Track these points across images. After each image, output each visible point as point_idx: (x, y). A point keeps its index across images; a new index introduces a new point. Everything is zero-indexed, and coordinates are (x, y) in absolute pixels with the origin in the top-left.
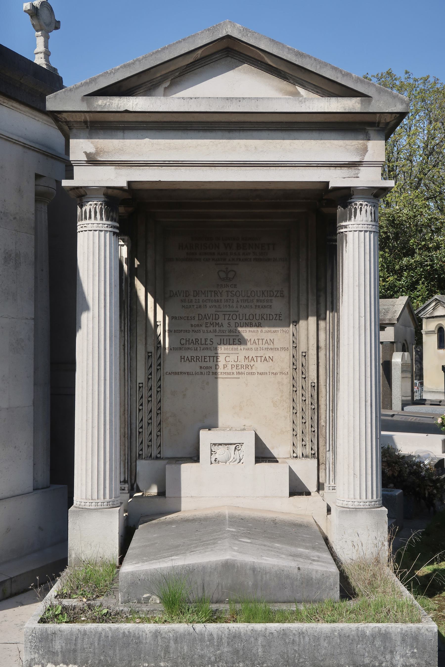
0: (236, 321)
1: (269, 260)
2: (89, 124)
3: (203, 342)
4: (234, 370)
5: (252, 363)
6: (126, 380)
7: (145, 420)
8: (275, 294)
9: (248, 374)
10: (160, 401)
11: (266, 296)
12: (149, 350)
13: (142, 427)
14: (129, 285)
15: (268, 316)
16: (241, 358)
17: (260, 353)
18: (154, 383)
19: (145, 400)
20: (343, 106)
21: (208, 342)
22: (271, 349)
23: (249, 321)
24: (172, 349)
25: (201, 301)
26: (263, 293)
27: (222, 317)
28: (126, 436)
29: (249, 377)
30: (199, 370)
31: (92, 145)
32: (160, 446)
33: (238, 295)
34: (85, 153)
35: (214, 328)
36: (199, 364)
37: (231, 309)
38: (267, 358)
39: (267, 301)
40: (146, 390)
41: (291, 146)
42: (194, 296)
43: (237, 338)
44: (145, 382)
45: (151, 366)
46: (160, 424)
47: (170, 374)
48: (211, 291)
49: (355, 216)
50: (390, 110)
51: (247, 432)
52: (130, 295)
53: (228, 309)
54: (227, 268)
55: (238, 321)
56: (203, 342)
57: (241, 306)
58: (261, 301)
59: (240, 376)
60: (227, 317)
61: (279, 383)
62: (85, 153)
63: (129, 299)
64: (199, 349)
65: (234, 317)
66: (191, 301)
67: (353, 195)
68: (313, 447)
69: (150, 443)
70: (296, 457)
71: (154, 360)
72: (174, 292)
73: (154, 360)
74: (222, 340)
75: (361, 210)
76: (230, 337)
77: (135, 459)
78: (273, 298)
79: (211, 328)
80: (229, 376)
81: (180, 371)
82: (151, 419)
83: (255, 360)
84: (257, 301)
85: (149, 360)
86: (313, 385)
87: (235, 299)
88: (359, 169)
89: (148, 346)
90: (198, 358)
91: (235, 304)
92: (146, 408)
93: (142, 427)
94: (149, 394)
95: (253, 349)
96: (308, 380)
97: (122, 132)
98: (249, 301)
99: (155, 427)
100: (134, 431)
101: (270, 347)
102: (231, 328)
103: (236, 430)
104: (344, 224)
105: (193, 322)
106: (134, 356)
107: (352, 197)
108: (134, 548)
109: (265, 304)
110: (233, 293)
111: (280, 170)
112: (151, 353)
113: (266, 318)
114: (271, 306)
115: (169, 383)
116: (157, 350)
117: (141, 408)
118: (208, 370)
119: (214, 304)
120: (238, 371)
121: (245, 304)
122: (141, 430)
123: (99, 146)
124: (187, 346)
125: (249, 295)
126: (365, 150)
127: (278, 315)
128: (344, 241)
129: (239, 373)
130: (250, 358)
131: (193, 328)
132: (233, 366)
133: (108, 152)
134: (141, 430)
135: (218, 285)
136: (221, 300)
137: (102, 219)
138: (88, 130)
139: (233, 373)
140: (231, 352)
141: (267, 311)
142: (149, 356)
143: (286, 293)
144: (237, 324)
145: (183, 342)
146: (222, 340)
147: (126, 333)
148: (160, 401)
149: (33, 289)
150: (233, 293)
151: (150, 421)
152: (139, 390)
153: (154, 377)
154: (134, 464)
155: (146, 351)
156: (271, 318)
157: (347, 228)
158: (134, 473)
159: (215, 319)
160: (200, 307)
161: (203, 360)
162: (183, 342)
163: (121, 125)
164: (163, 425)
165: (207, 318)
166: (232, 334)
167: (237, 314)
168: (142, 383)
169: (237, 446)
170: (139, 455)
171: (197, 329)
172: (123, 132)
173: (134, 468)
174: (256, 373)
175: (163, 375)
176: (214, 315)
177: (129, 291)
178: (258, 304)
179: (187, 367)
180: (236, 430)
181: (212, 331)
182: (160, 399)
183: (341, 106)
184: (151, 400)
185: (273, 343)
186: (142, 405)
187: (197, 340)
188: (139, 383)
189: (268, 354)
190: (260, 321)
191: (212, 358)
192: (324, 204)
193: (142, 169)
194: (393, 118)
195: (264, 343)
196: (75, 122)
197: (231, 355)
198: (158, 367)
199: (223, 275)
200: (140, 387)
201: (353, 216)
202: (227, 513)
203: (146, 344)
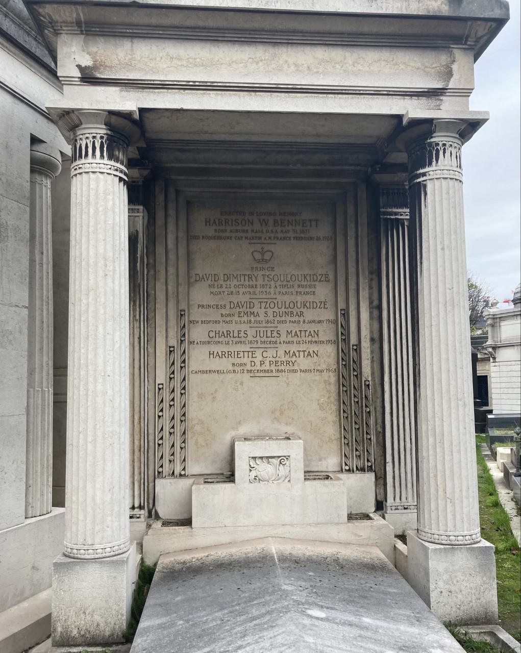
0: (274, 310)
1: (311, 238)
2: (83, 25)
3: (236, 335)
4: (273, 368)
5: (294, 359)
6: (142, 380)
7: (167, 429)
8: (319, 277)
9: (290, 371)
10: (184, 406)
11: (309, 280)
12: (171, 345)
13: (162, 438)
14: (145, 266)
15: (311, 304)
16: (281, 353)
17: (303, 347)
18: (177, 384)
19: (166, 405)
20: (426, 7)
21: (242, 334)
22: (316, 342)
23: (290, 310)
24: (199, 343)
25: (232, 286)
26: (305, 277)
27: (257, 305)
28: (142, 449)
29: (291, 375)
30: (231, 368)
31: (88, 57)
32: (184, 460)
33: (276, 279)
34: (79, 66)
35: (249, 318)
36: (232, 360)
37: (268, 296)
38: (311, 352)
39: (310, 286)
40: (168, 393)
41: (354, 66)
42: (224, 281)
43: (276, 329)
44: (166, 382)
45: (173, 363)
46: (184, 433)
47: (196, 372)
48: (244, 275)
49: (437, 160)
50: (486, 14)
51: (294, 441)
52: (147, 278)
53: (264, 296)
54: (262, 248)
55: (276, 309)
56: (236, 335)
57: (280, 292)
58: (303, 286)
59: (280, 374)
60: (263, 305)
61: (325, 382)
62: (79, 66)
63: (146, 282)
64: (231, 342)
65: (272, 305)
66: (221, 286)
67: (435, 132)
68: (369, 458)
69: (172, 457)
70: (349, 470)
71: (177, 356)
72: (201, 276)
73: (177, 356)
74: (258, 332)
75: (444, 152)
76: (267, 329)
77: (153, 478)
78: (317, 283)
79: (245, 318)
80: (267, 375)
81: (208, 369)
82: (173, 427)
83: (297, 355)
84: (299, 286)
85: (171, 356)
86: (367, 383)
87: (272, 283)
88: (441, 100)
89: (169, 339)
90: (229, 354)
91: (272, 290)
92: (167, 414)
93: (162, 438)
94: (171, 397)
95: (295, 342)
96: (361, 378)
97: (130, 40)
98: (289, 286)
99: (178, 438)
100: (151, 444)
101: (314, 339)
102: (268, 318)
103: (277, 439)
104: (422, 171)
105: (224, 312)
106: (151, 350)
107: (433, 135)
108: (147, 630)
109: (308, 290)
110: (270, 277)
111: (340, 98)
112: (174, 347)
113: (308, 306)
114: (314, 292)
115: (194, 382)
116: (181, 344)
117: (160, 414)
118: (242, 368)
119: (248, 290)
120: (277, 368)
121: (284, 290)
122: (160, 442)
123: (98, 58)
124: (217, 339)
125: (289, 279)
126: (449, 74)
127: (323, 303)
128: (422, 193)
129: (278, 370)
130: (291, 353)
131: (224, 318)
132: (271, 363)
133: (111, 67)
134: (160, 442)
135: (252, 268)
136: (256, 285)
137: (102, 156)
138: (83, 36)
139: (272, 371)
140: (269, 346)
141: (310, 298)
142: (171, 351)
143: (331, 277)
144: (275, 314)
145: (212, 334)
146: (258, 332)
147: (142, 323)
148: (184, 406)
149: (28, 271)
150: (270, 277)
151: (172, 431)
152: (158, 393)
153: (178, 377)
154: (151, 485)
155: (167, 345)
156: (315, 306)
157: (426, 175)
158: (151, 496)
159: (250, 308)
160: (232, 293)
161: (236, 356)
162: (212, 334)
163: (128, 31)
164: (189, 435)
165: (241, 306)
166: (269, 325)
167: (276, 302)
168: (162, 384)
169: (282, 460)
170: (159, 473)
171: (228, 319)
172: (132, 41)
173: (151, 490)
174: (299, 371)
175: (188, 375)
176: (248, 303)
177: (145, 273)
178: (299, 290)
179: (216, 364)
180: (277, 439)
181: (246, 322)
182: (185, 404)
183: (423, 7)
184: (174, 405)
185: (318, 335)
186: (162, 410)
187: (229, 333)
188: (159, 384)
189: (313, 348)
190: (302, 310)
191: (246, 354)
192: (378, 169)
193: (158, 92)
194: (486, 31)
195: (307, 335)
196: (64, 22)
197: (268, 350)
198: (183, 365)
199: (258, 256)
200: (159, 389)
201: (434, 160)
202: (274, 551)
203: (167, 337)
